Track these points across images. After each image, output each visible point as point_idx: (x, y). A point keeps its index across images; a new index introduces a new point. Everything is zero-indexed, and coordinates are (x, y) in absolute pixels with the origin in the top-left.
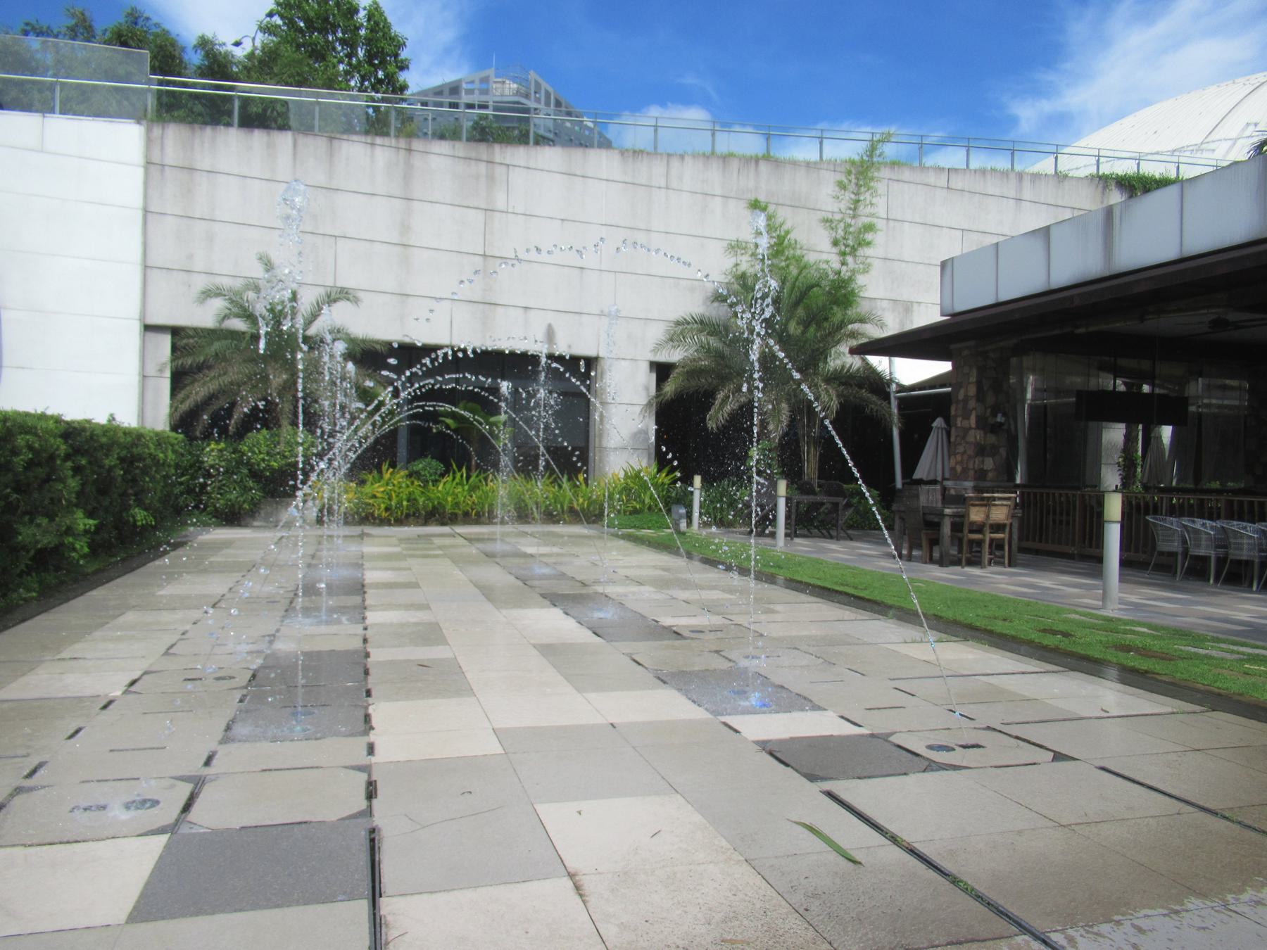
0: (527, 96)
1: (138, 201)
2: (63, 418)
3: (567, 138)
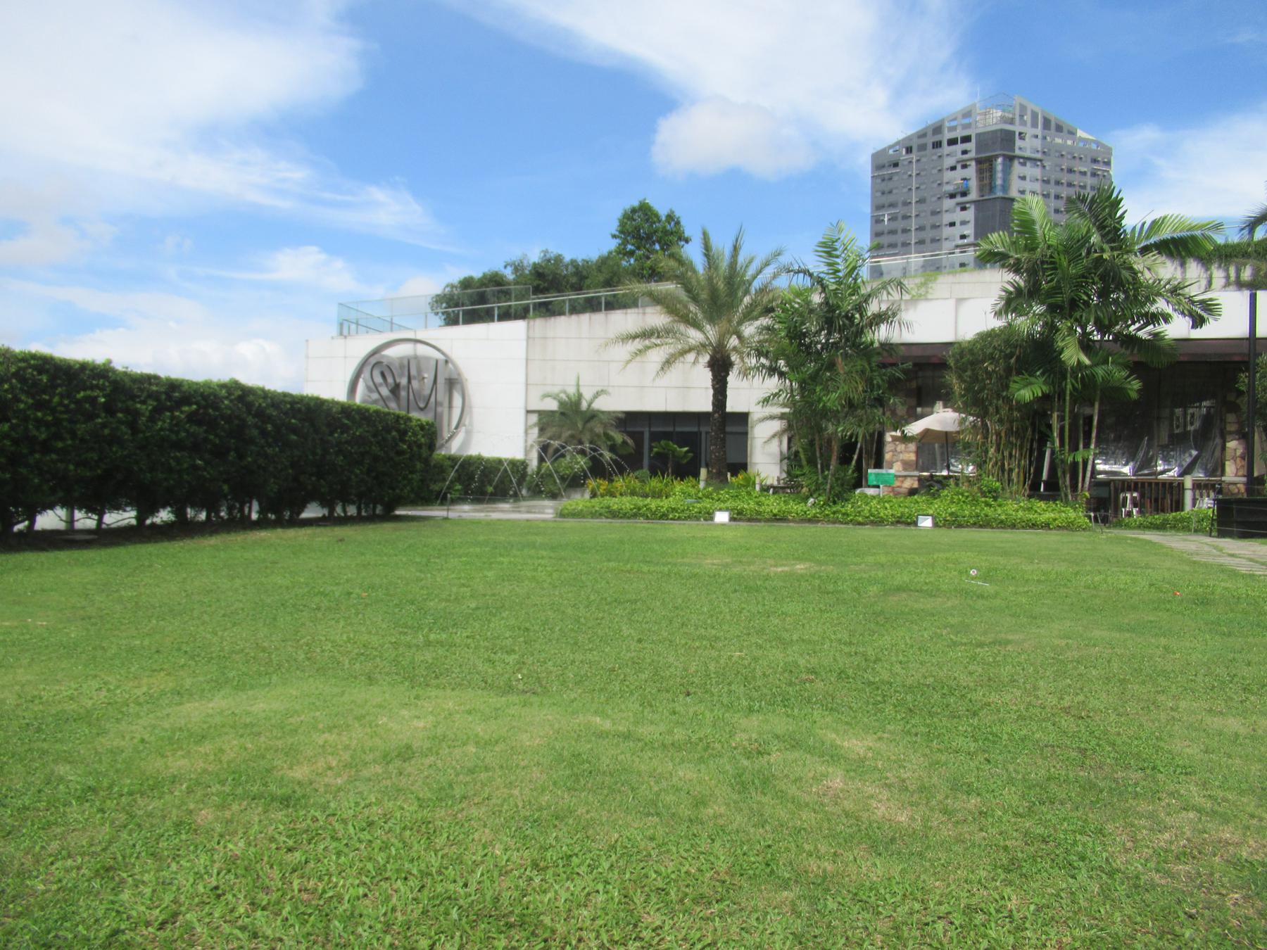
0: (1012, 122)
1: (523, 356)
2: (112, 365)
3: (1057, 154)
